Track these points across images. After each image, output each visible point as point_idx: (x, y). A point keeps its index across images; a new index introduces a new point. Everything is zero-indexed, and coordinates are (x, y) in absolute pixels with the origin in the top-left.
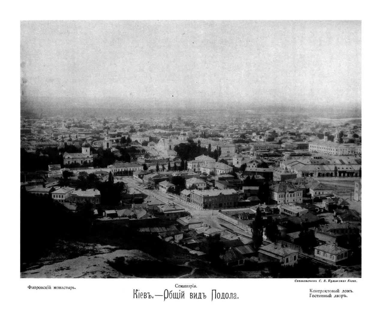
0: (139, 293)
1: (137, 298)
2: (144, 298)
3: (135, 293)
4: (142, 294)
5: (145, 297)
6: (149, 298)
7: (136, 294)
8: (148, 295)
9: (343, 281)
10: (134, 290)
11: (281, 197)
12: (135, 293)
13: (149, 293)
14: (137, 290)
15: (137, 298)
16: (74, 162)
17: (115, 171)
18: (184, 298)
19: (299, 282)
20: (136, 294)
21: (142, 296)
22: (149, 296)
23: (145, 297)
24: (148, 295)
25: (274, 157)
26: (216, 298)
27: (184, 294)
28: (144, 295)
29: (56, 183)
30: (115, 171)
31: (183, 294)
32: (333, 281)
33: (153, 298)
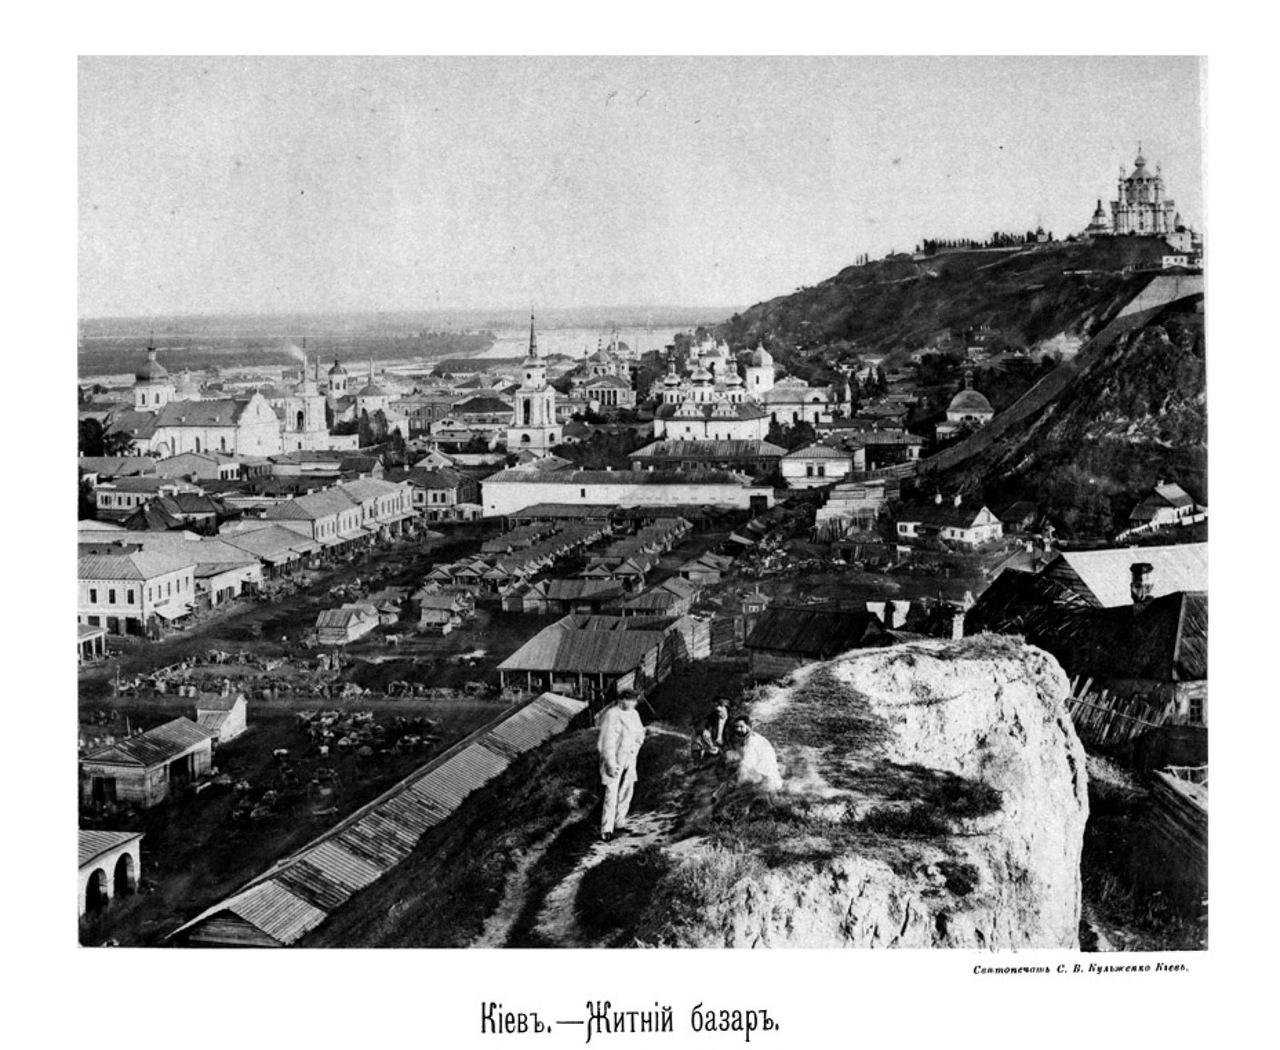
0: (501, 1015)
1: (493, 1031)
2: (520, 1031)
3: (487, 1014)
4: (510, 1019)
5: (523, 1027)
6: (765, 1028)
7: (494, 1019)
8: (531, 1022)
9: (1141, 968)
10: (484, 1004)
11: (94, 644)
12: (487, 1014)
13: (765, 1012)
14: (493, 1005)
15: (493, 1031)
16: (360, 414)
17: (702, 399)
18: (671, 1030)
19: (1138, 972)
20: (494, 1019)
21: (511, 1027)
22: (537, 1024)
23: (523, 1027)
24: (531, 1022)
25: (211, 352)
26: (484, 1031)
27: (670, 1017)
28: (520, 1023)
29: (480, 529)
30: (702, 399)
31: (667, 1015)
32: (1106, 969)
33: (549, 1030)
